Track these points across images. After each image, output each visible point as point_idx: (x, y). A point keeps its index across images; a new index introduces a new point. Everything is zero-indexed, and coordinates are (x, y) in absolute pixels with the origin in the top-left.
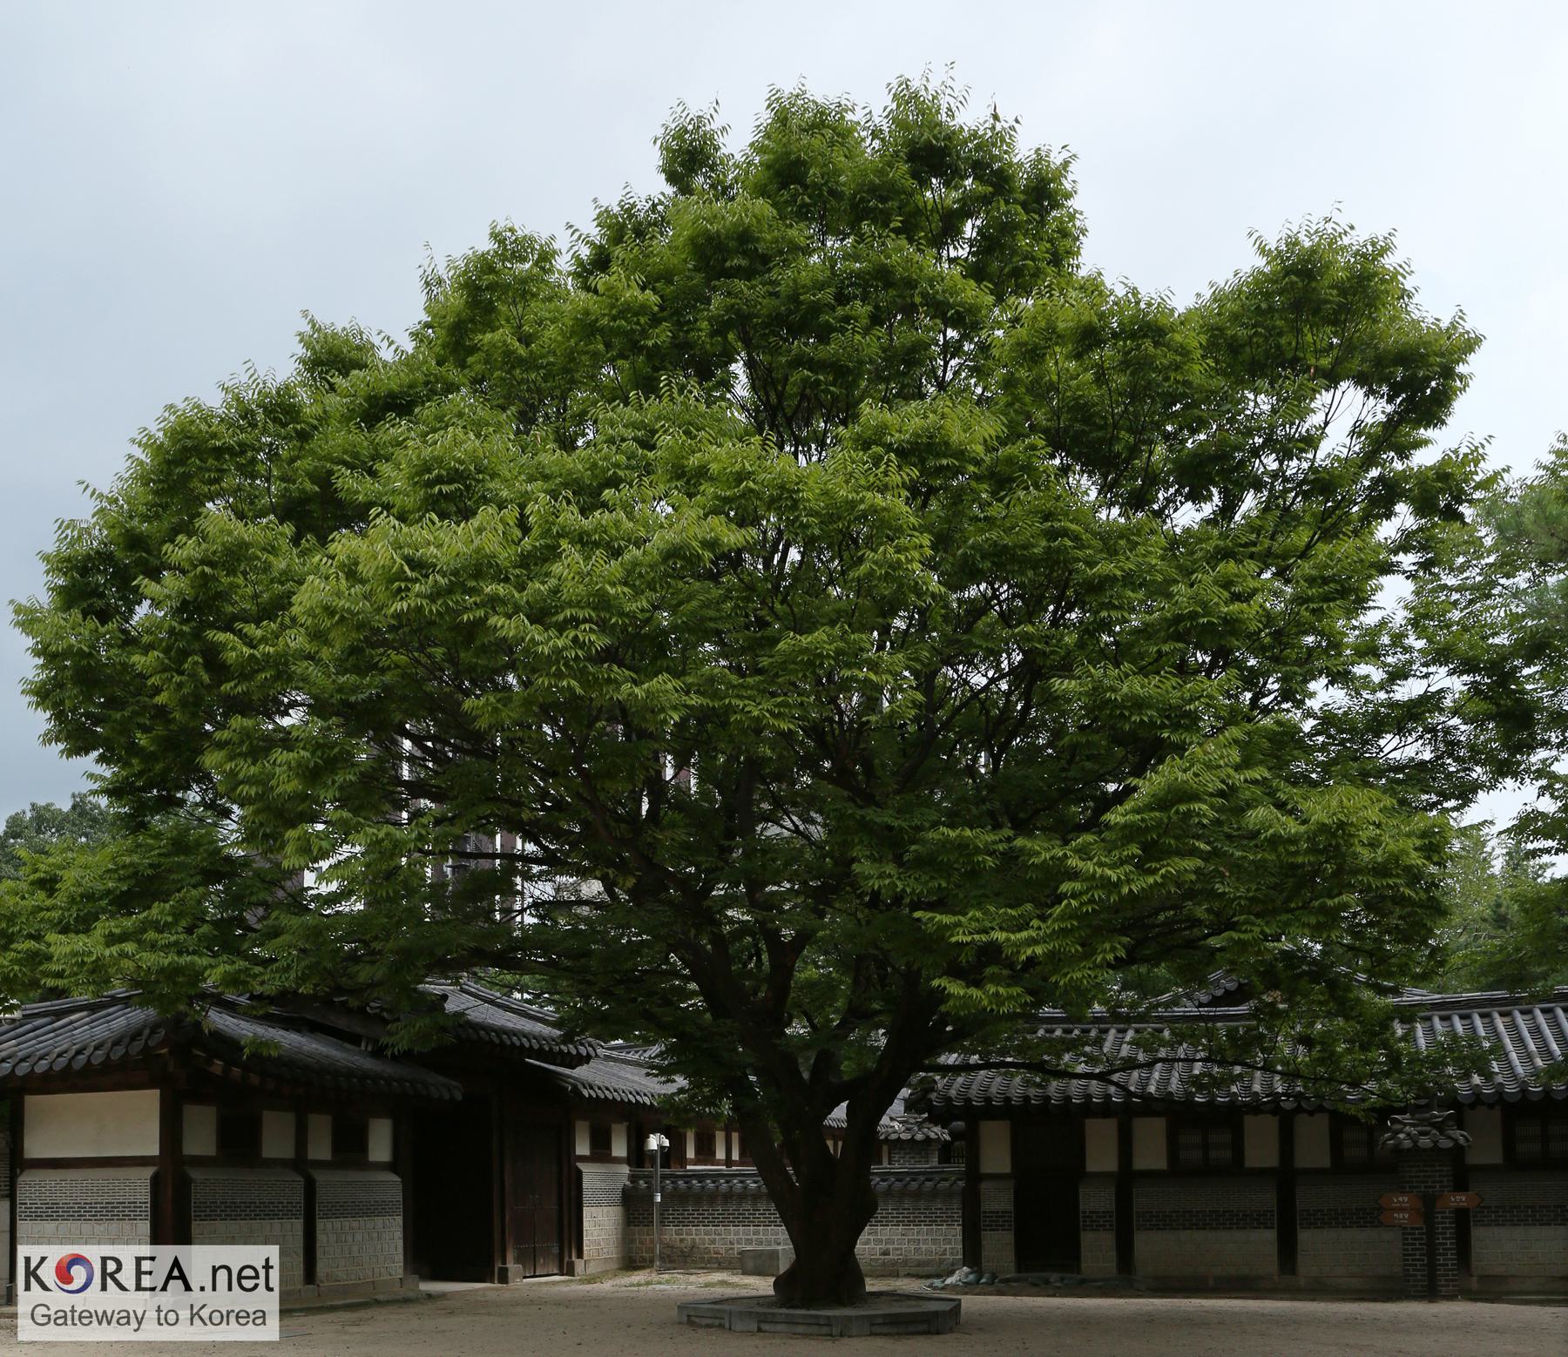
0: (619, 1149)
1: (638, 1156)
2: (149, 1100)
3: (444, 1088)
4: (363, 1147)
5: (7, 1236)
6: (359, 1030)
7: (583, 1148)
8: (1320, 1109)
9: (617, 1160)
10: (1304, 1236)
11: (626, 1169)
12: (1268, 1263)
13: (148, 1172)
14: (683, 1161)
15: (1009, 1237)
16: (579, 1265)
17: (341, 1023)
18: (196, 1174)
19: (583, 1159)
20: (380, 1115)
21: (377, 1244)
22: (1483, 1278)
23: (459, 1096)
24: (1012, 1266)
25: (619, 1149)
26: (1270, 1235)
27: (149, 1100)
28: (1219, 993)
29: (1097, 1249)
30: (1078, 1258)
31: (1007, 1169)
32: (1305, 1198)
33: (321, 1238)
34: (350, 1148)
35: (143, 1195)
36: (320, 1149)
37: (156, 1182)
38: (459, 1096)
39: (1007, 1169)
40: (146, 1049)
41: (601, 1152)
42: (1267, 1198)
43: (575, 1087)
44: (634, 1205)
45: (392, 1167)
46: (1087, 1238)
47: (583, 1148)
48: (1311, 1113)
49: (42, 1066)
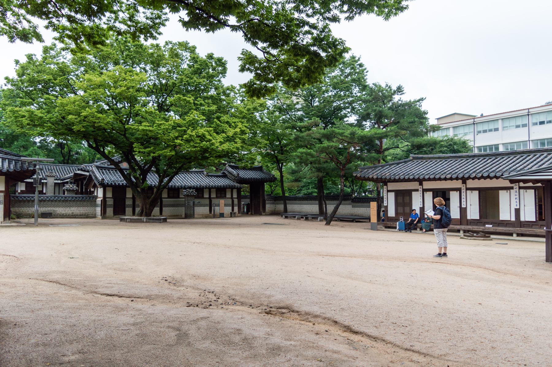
5: (422, 198)
15: (112, 209)
31: (111, 196)
42: (207, 201)
46: (127, 209)
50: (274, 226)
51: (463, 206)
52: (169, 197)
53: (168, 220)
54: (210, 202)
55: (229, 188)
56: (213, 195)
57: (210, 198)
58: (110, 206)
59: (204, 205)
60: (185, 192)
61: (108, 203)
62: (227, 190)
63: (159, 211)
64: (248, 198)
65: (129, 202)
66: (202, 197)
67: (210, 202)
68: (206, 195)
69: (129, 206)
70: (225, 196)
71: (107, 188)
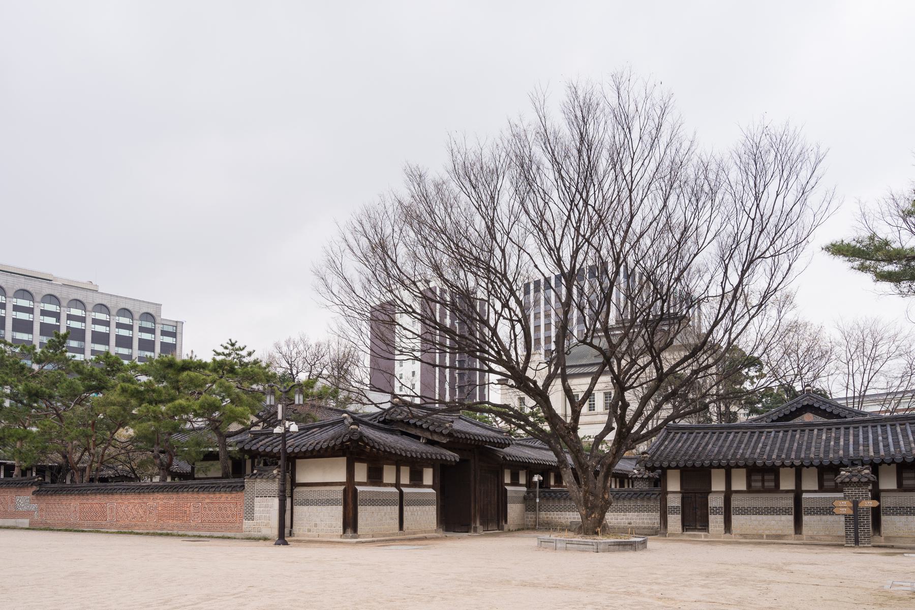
0: (522, 481)
1: (530, 484)
2: (342, 461)
3: (451, 456)
4: (421, 479)
5: (397, 521)
6: (419, 434)
7: (507, 480)
8: (812, 465)
9: (521, 485)
10: (806, 518)
11: (525, 489)
12: (791, 529)
13: (342, 488)
14: (548, 487)
15: (679, 517)
16: (506, 527)
17: (413, 431)
18: (360, 489)
19: (508, 485)
20: (428, 467)
21: (425, 516)
22: (888, 538)
23: (458, 460)
24: (680, 529)
25: (522, 481)
26: (791, 518)
27: (342, 461)
28: (781, 415)
29: (716, 522)
30: (708, 526)
31: (679, 490)
32: (736, 502)
33: (405, 514)
34: (416, 480)
35: (340, 496)
36: (405, 479)
37: (345, 490)
38: (458, 460)
39: (679, 490)
40: (342, 443)
41: (515, 482)
42: (789, 502)
43: (504, 457)
44: (528, 501)
45: (433, 487)
46: (711, 518)
47: (507, 480)
48: (808, 467)
49: (304, 449)
50: (317, 545)
51: (445, 441)
52: (750, 490)
53: (649, 544)
54: (798, 501)
55: (719, 467)
56: (739, 484)
57: (798, 495)
58: (674, 510)
59: (785, 511)
60: (26, 522)
61: (669, 504)
62: (714, 472)
63: (792, 524)
64: (394, 504)
65: (715, 501)
66: (776, 489)
67: (798, 501)
68: (787, 484)
69: (716, 511)
70: (777, 485)
71: (734, 471)
